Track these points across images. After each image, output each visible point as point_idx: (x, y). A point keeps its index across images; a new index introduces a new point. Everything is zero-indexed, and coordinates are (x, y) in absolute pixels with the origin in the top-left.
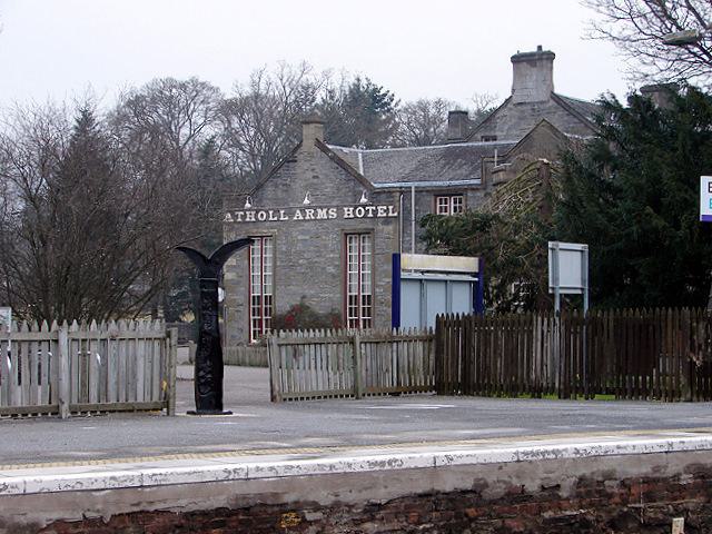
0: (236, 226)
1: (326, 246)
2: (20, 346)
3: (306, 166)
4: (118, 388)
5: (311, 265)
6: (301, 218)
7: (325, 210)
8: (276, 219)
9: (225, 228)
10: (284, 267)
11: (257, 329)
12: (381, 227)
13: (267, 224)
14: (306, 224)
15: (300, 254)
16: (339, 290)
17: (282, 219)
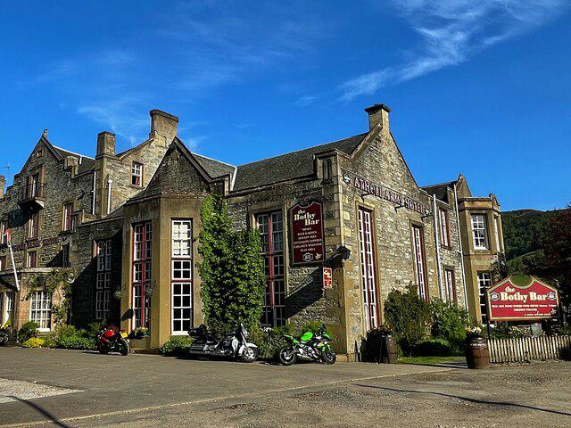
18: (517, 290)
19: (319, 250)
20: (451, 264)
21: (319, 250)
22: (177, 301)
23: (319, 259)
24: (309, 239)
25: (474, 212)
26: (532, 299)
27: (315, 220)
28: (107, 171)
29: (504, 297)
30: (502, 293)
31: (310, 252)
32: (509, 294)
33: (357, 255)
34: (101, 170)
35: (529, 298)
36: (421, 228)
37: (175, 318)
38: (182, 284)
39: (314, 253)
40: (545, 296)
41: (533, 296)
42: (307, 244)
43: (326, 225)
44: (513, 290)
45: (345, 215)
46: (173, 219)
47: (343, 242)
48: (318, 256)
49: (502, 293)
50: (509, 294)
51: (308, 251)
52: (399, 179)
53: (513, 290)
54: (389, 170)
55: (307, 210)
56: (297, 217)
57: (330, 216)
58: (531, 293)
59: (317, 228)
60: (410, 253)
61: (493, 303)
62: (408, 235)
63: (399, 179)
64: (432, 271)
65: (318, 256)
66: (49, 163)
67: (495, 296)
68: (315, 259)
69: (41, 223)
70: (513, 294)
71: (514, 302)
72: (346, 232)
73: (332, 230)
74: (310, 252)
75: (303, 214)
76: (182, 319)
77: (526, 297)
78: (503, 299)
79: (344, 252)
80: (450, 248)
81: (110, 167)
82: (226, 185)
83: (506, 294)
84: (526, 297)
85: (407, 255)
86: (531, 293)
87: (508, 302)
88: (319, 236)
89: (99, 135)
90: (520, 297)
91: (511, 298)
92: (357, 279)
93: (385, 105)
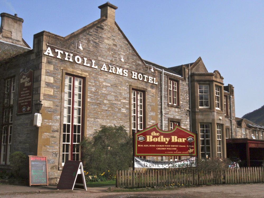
0: (54, 60)
1: (121, 94)
2: (221, 183)
3: (109, 35)
4: (18, 193)
5: (112, 105)
6: (106, 70)
7: (121, 69)
8: (89, 65)
9: (44, 60)
10: (93, 104)
11: (5, 135)
12: (149, 89)
13: (81, 67)
14: (109, 76)
15: (105, 96)
16: (88, 111)
17: (93, 66)
18: (161, 134)
20: (177, 117)
26: (173, 141)
29: (149, 139)
30: (148, 137)
32: (154, 137)
35: (170, 140)
36: (144, 92)
40: (184, 140)
41: (174, 139)
44: (158, 134)
49: (148, 137)
50: (154, 137)
53: (158, 134)
58: (173, 137)
60: (127, 109)
61: (139, 143)
62: (127, 96)
67: (141, 139)
70: (157, 137)
71: (157, 143)
77: (168, 139)
83: (151, 137)
85: (124, 110)
86: (173, 137)
87: (153, 143)
90: (163, 139)
91: (156, 140)
93: (112, 3)
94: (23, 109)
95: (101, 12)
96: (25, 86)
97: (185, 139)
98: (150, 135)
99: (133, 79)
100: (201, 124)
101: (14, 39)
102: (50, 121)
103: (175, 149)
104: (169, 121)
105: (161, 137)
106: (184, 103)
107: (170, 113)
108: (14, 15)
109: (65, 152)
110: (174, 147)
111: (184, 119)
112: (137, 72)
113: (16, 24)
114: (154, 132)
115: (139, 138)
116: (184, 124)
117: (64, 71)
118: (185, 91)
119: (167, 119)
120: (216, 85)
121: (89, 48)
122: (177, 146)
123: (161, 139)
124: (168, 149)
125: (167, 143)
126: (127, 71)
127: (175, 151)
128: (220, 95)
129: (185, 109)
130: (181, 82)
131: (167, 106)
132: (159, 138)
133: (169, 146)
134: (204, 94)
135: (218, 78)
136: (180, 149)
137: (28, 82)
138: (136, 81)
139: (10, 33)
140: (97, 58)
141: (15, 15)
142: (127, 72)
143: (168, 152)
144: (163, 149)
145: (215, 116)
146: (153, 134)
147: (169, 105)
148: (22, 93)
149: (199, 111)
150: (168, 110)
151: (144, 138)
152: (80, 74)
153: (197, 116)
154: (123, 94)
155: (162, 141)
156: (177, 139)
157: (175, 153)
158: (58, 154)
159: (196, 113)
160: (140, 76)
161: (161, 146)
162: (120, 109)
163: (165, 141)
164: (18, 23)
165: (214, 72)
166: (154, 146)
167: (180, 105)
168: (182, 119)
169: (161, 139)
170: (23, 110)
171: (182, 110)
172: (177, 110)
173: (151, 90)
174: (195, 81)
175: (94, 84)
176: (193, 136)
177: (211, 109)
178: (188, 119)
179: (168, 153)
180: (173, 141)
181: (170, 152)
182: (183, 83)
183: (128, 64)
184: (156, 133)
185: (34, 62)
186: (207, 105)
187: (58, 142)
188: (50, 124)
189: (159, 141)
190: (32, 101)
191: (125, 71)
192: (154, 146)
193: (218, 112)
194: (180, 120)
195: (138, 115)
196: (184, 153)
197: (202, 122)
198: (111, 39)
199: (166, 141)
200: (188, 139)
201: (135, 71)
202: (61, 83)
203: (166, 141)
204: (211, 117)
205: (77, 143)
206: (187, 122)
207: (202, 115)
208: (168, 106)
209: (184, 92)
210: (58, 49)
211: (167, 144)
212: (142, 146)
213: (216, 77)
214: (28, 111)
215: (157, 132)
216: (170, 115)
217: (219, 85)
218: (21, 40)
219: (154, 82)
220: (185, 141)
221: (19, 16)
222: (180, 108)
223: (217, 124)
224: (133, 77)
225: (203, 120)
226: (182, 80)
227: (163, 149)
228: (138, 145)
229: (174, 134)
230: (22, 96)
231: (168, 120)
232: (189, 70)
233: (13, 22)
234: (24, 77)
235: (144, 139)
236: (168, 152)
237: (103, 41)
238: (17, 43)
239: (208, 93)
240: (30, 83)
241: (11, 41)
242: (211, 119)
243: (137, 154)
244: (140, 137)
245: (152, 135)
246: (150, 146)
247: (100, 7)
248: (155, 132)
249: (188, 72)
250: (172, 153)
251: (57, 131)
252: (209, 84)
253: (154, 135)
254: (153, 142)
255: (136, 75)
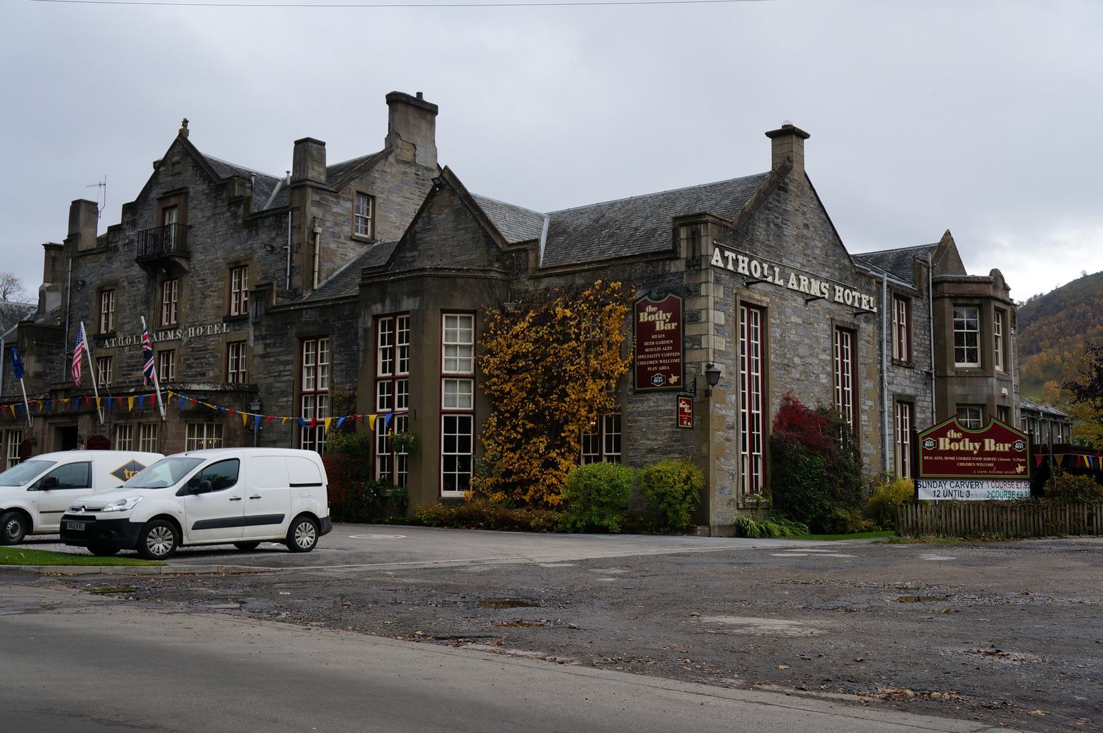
18: (965, 435)
19: (676, 369)
20: (909, 391)
21: (676, 369)
22: (450, 445)
23: (675, 384)
24: (661, 352)
25: (960, 301)
26: (987, 449)
27: (670, 322)
28: (312, 210)
29: (944, 444)
30: (941, 440)
31: (662, 372)
32: (952, 440)
33: (733, 378)
34: (301, 209)
35: (983, 446)
36: (854, 332)
37: (400, 329)
38: (457, 416)
39: (667, 374)
40: (1007, 446)
41: (990, 444)
42: (658, 359)
43: (691, 330)
44: (959, 435)
45: (718, 317)
46: (443, 311)
47: (711, 359)
48: (673, 379)
49: (941, 440)
50: (952, 440)
51: (658, 371)
52: (818, 252)
53: (959, 435)
54: (800, 238)
55: (660, 307)
56: (644, 317)
57: (695, 318)
58: (987, 441)
59: (676, 337)
60: (828, 374)
61: (926, 452)
62: (828, 344)
63: (818, 252)
64: (870, 403)
65: (673, 379)
66: (198, 188)
67: (929, 444)
68: (668, 383)
69: (186, 291)
70: (958, 440)
72: (717, 342)
73: (697, 340)
74: (662, 372)
75: (654, 313)
76: (386, 395)
77: (977, 445)
78: (942, 448)
79: (712, 376)
80: (909, 365)
81: (318, 204)
82: (531, 257)
83: (947, 441)
84: (977, 445)
86: (987, 441)
87: (950, 453)
88: (676, 347)
89: (297, 143)
90: (968, 445)
91: (955, 447)
92: (730, 415)
94: (653, 378)
95: (773, 146)
96: (658, 329)
97: (1010, 445)
98: (946, 436)
99: (770, 285)
100: (959, 407)
101: (422, 166)
102: (723, 406)
103: (991, 465)
104: (895, 401)
105: (964, 441)
106: (920, 355)
107: (895, 382)
108: (415, 96)
109: (457, 475)
110: (990, 462)
111: (921, 396)
112: (842, 286)
113: (424, 122)
114: (952, 431)
115: (925, 442)
116: (921, 407)
117: (739, 298)
118: (921, 322)
119: (891, 397)
120: (997, 309)
121: (768, 241)
122: (995, 459)
123: (964, 446)
124: (978, 464)
125: (975, 452)
126: (827, 286)
127: (991, 469)
128: (1003, 334)
129: (921, 371)
130: (914, 301)
131: (891, 364)
132: (961, 443)
133: (980, 459)
134: (966, 331)
135: (1000, 290)
136: (1000, 466)
137: (667, 321)
138: (840, 308)
139: (412, 148)
140: (781, 261)
141: (420, 94)
142: (828, 287)
143: (978, 472)
144: (969, 464)
145: (994, 387)
146: (951, 435)
147: (894, 362)
148: (646, 344)
149: (953, 374)
150: (893, 375)
151: (934, 442)
152: (758, 300)
153: (949, 387)
154: (822, 340)
155: (967, 449)
156: (995, 445)
157: (991, 474)
158: (736, 476)
159: (949, 380)
160: (755, 266)
161: (964, 459)
162: (817, 376)
163: (972, 449)
164: (427, 118)
165: (991, 274)
166: (953, 458)
167: (914, 359)
168: (917, 396)
169: (964, 446)
170: (655, 381)
171: (917, 374)
172: (907, 372)
173: (865, 328)
174: (947, 297)
175: (778, 322)
176: (1025, 440)
177: (985, 371)
178: (928, 395)
179: (1006, 474)
180: (987, 449)
181: (982, 472)
182: (918, 304)
183: (827, 269)
184: (955, 434)
185: (682, 278)
186: (972, 359)
187: (734, 452)
188: (724, 412)
189: (962, 448)
190: (684, 364)
191: (825, 287)
192: (953, 458)
193: (1001, 377)
194: (914, 397)
195: (752, 373)
196: (1007, 474)
197: (962, 402)
198: (800, 213)
199: (975, 448)
200: (1015, 444)
201: (839, 285)
202: (734, 325)
203: (975, 448)
204: (986, 391)
205: (404, 454)
206: (926, 401)
207: (964, 385)
208: (893, 364)
209: (919, 327)
210: (729, 250)
211: (977, 456)
212: (931, 458)
213: (996, 287)
214: (673, 385)
215: (957, 431)
216: (895, 386)
217: (1002, 307)
218: (434, 167)
219: (774, 279)
220: (1009, 448)
221: (427, 98)
222: (913, 368)
223: (999, 406)
224: (836, 299)
225: (965, 396)
226: (916, 296)
227: (969, 464)
228: (923, 458)
229: (988, 435)
230: (647, 350)
231: (893, 397)
232: (928, 268)
233: (418, 116)
234: (650, 309)
235: (934, 446)
236: (978, 472)
237: (788, 221)
238: (427, 175)
239: (976, 329)
240: (674, 325)
241: (414, 171)
242: (984, 396)
243: (922, 475)
244: (928, 440)
245: (949, 436)
246: (946, 458)
247: (769, 134)
248: (954, 432)
249: (926, 274)
250: (983, 474)
251: (732, 428)
252: (979, 306)
253: (952, 436)
254: (950, 450)
255: (746, 265)
